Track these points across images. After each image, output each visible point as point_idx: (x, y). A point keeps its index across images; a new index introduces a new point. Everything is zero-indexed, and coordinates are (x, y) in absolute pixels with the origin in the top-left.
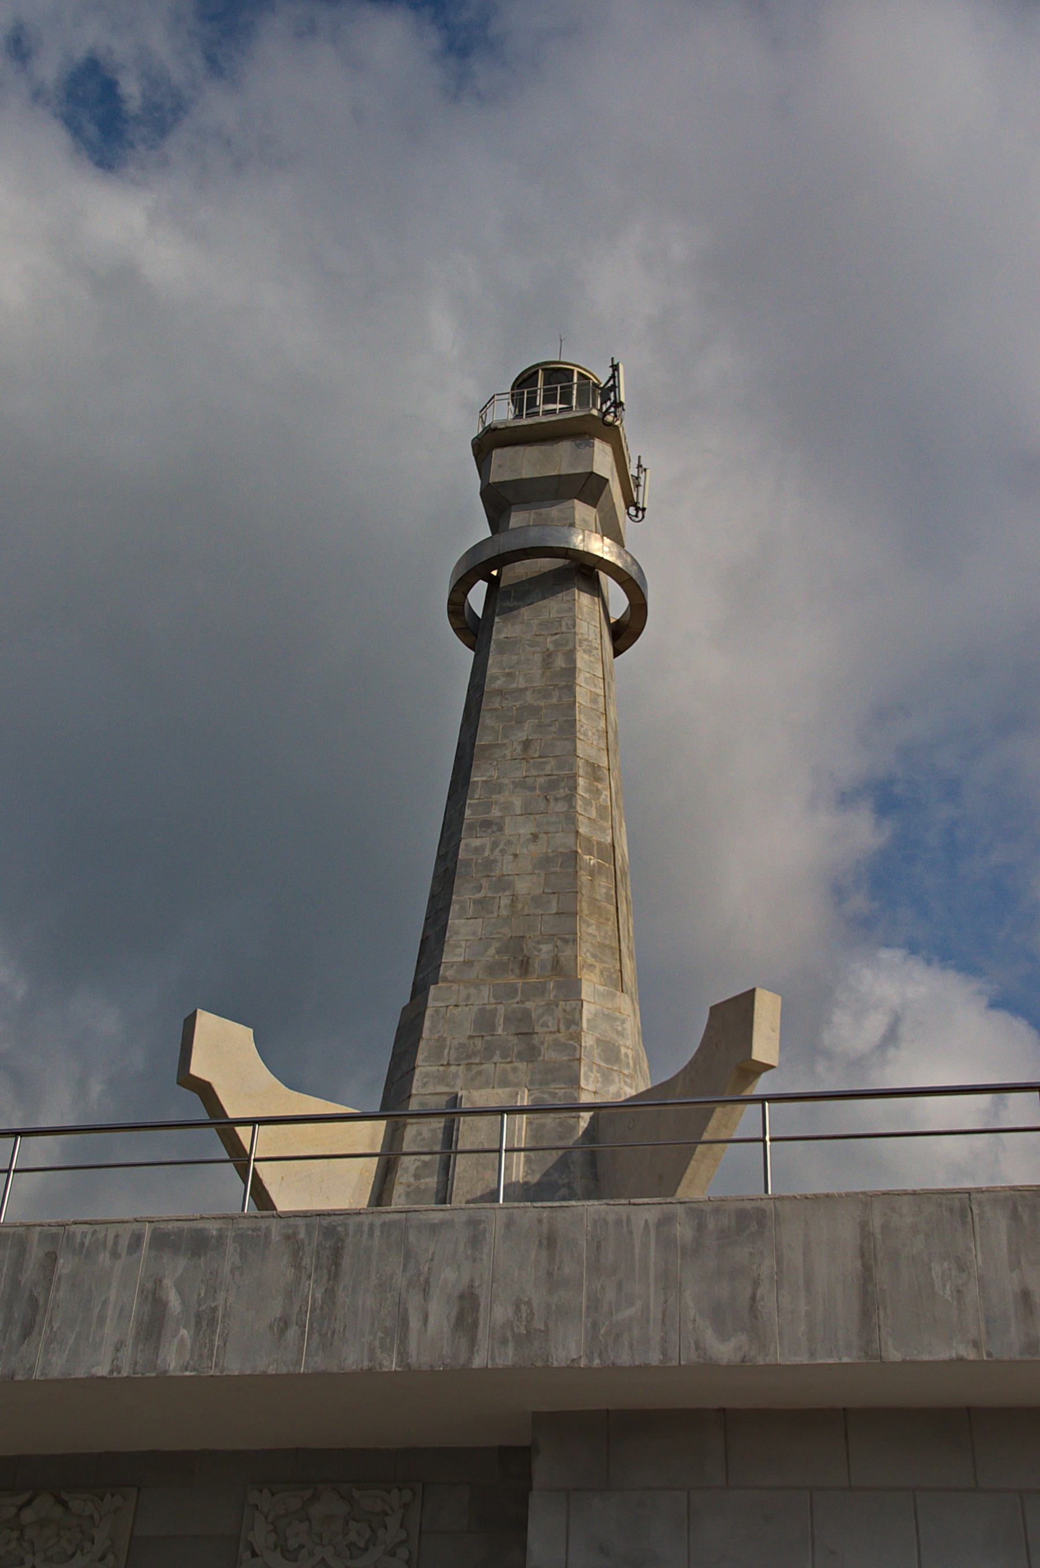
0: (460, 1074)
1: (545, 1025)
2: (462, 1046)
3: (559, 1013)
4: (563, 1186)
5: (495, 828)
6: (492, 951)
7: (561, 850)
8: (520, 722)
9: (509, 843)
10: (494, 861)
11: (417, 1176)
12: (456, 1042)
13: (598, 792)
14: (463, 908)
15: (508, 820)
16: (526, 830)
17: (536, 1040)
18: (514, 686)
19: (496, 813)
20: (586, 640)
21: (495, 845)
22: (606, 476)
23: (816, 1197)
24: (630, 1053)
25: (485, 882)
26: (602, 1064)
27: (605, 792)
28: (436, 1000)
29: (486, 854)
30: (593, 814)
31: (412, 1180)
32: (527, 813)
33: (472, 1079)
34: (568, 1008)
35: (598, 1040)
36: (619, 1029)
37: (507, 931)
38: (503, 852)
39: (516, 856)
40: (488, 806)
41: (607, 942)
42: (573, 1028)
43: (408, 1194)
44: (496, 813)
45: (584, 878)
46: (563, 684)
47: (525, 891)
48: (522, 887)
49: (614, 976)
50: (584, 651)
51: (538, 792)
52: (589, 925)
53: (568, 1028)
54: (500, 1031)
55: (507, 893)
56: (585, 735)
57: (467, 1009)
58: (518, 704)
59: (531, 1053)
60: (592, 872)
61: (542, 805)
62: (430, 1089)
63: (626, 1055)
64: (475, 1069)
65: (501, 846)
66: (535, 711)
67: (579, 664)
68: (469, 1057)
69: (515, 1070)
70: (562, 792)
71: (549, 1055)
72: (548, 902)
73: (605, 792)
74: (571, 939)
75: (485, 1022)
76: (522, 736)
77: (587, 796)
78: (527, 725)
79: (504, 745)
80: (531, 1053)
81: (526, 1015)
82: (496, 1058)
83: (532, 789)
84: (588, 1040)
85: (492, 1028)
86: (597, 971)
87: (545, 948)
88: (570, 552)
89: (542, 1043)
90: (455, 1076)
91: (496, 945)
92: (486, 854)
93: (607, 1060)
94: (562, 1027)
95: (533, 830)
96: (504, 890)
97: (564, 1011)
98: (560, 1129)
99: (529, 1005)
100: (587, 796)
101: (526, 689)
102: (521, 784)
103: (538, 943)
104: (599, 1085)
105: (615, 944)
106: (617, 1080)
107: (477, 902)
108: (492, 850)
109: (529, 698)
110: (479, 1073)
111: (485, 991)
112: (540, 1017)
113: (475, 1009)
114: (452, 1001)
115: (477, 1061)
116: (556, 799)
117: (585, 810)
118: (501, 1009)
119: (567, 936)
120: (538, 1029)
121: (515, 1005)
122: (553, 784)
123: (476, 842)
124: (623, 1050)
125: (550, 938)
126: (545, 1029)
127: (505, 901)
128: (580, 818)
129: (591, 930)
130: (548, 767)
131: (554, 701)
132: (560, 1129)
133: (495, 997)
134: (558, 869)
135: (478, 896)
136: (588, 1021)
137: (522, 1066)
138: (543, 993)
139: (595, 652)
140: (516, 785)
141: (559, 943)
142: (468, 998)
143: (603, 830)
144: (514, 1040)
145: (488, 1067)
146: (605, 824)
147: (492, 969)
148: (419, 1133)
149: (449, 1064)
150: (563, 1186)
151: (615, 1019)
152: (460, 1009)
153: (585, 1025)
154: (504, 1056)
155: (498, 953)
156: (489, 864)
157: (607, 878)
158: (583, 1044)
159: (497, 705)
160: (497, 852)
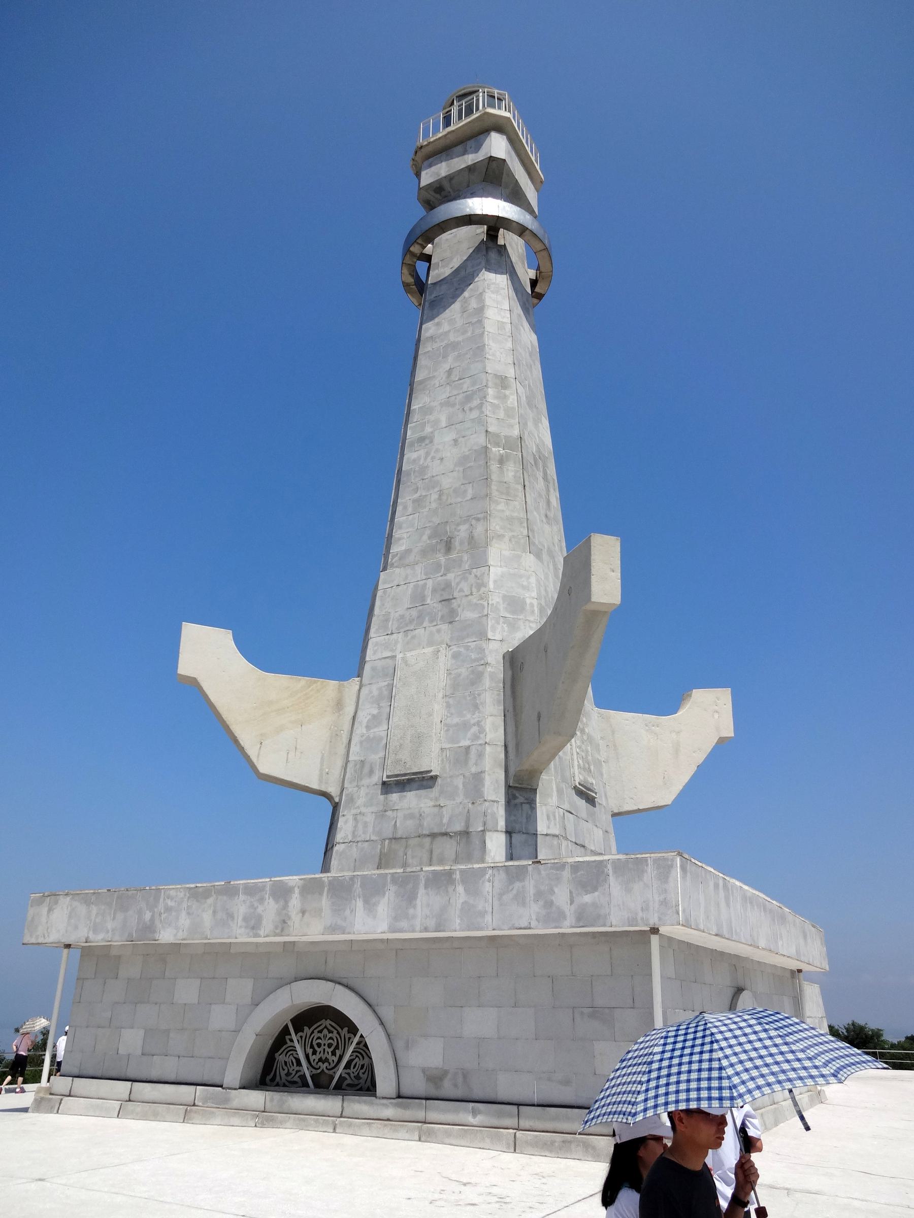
0: (400, 640)
1: (461, 590)
2: (402, 617)
3: (471, 579)
4: (474, 725)
5: (427, 441)
6: (425, 537)
7: (476, 448)
8: (445, 357)
9: (437, 451)
10: (427, 467)
11: (368, 728)
12: (397, 615)
13: (505, 397)
14: (405, 508)
15: (436, 433)
16: (449, 437)
17: (455, 604)
18: (441, 331)
19: (428, 429)
20: (493, 283)
21: (427, 454)
22: (503, 158)
23: (224, 1073)
24: (535, 602)
25: (420, 484)
26: (508, 615)
27: (512, 397)
28: (385, 583)
29: (421, 463)
30: (502, 415)
31: (364, 731)
32: (450, 425)
33: (408, 643)
34: (478, 574)
35: (505, 597)
36: (525, 583)
37: (436, 520)
38: (433, 458)
39: (442, 459)
40: (423, 426)
41: (515, 514)
42: (483, 589)
43: (361, 743)
44: (428, 429)
45: (494, 466)
46: (476, 320)
47: (447, 486)
48: (446, 482)
49: (522, 541)
50: (493, 292)
51: (457, 407)
52: (498, 503)
53: (479, 590)
54: (428, 601)
55: (436, 489)
56: (494, 355)
57: (405, 587)
58: (443, 344)
59: (451, 618)
60: (502, 461)
61: (461, 416)
62: (379, 655)
63: (532, 605)
64: (410, 634)
65: (432, 454)
66: (454, 346)
67: (488, 302)
68: (407, 625)
69: (439, 631)
70: (476, 402)
71: (468, 615)
72: (465, 491)
73: (512, 397)
74: (485, 516)
75: (419, 598)
76: (447, 367)
77: (495, 402)
78: (450, 359)
79: (434, 377)
80: (451, 618)
81: (448, 586)
82: (426, 624)
83: (453, 405)
84: (496, 599)
85: (423, 598)
86: (507, 539)
87: (463, 528)
88: (473, 218)
89: (459, 606)
90: (396, 642)
91: (428, 532)
92: (421, 463)
93: (514, 612)
94: (474, 590)
95: (454, 436)
96: (433, 488)
97: (476, 576)
98: (472, 676)
99: (450, 576)
100: (495, 402)
101: (449, 331)
102: (447, 403)
103: (458, 525)
104: (505, 634)
105: (522, 515)
106: (522, 627)
107: (414, 501)
108: (426, 459)
109: (452, 338)
110: (413, 637)
111: (419, 569)
112: (458, 584)
113: (411, 585)
114: (396, 583)
115: (412, 628)
116: (471, 409)
117: (494, 413)
118: (430, 583)
119: (479, 516)
120: (456, 594)
121: (440, 578)
122: (469, 398)
123: (414, 455)
124: (528, 601)
125: (467, 519)
126: (462, 594)
127: (435, 496)
128: (489, 420)
129: (500, 507)
130: (465, 386)
131: (469, 334)
132: (472, 676)
133: (426, 575)
134: (472, 464)
135: (416, 496)
136: (495, 582)
137: (444, 627)
138: (460, 566)
139: (502, 291)
140: (442, 405)
141: (474, 522)
142: (406, 577)
143: (511, 426)
144: (439, 606)
145: (420, 632)
146: (512, 421)
147: (424, 553)
148: (371, 692)
149: (392, 634)
150: (474, 725)
151: (521, 576)
152: (400, 588)
153: (491, 585)
154: (431, 621)
155: (429, 538)
156: (423, 470)
157: (515, 463)
158: (490, 602)
159: (430, 349)
160: (429, 459)
